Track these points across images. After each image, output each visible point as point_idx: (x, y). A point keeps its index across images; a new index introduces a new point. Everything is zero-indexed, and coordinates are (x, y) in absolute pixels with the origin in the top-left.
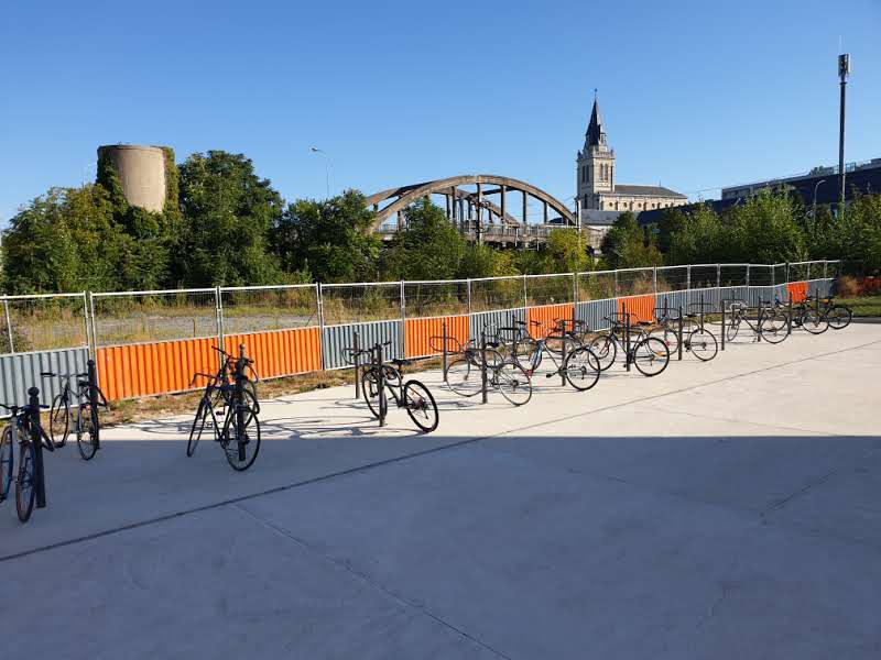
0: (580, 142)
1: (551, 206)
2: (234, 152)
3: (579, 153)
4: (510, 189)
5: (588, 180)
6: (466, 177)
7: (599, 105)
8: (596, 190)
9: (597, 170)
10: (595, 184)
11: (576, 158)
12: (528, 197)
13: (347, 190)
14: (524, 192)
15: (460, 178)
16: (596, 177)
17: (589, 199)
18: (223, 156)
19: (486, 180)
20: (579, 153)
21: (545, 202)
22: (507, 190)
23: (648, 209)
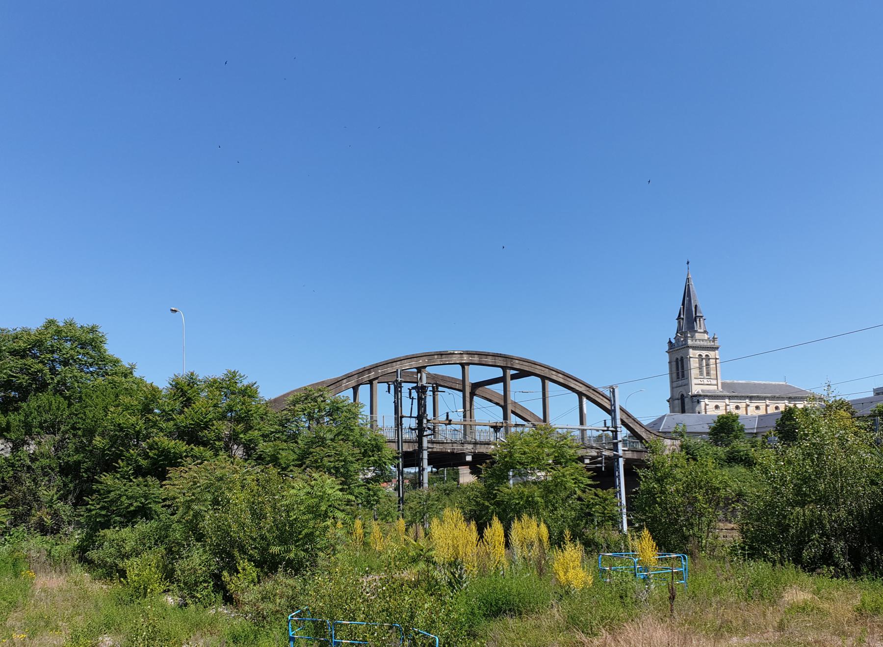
0: (671, 331)
1: (589, 398)
2: (125, 363)
3: (670, 342)
4: (523, 374)
5: (683, 376)
6: (441, 354)
7: (693, 288)
8: (695, 389)
9: (694, 363)
10: (694, 381)
11: (667, 348)
12: (549, 384)
13: (172, 376)
14: (544, 378)
15: (430, 355)
16: (694, 373)
17: (686, 400)
18: (192, 381)
19: (476, 359)
20: (670, 342)
21: (580, 395)
22: (514, 377)
23: (769, 412)
